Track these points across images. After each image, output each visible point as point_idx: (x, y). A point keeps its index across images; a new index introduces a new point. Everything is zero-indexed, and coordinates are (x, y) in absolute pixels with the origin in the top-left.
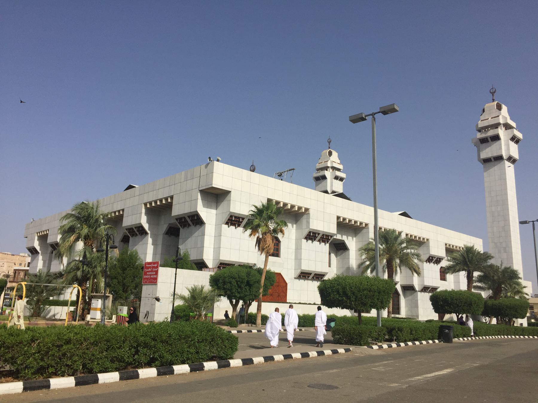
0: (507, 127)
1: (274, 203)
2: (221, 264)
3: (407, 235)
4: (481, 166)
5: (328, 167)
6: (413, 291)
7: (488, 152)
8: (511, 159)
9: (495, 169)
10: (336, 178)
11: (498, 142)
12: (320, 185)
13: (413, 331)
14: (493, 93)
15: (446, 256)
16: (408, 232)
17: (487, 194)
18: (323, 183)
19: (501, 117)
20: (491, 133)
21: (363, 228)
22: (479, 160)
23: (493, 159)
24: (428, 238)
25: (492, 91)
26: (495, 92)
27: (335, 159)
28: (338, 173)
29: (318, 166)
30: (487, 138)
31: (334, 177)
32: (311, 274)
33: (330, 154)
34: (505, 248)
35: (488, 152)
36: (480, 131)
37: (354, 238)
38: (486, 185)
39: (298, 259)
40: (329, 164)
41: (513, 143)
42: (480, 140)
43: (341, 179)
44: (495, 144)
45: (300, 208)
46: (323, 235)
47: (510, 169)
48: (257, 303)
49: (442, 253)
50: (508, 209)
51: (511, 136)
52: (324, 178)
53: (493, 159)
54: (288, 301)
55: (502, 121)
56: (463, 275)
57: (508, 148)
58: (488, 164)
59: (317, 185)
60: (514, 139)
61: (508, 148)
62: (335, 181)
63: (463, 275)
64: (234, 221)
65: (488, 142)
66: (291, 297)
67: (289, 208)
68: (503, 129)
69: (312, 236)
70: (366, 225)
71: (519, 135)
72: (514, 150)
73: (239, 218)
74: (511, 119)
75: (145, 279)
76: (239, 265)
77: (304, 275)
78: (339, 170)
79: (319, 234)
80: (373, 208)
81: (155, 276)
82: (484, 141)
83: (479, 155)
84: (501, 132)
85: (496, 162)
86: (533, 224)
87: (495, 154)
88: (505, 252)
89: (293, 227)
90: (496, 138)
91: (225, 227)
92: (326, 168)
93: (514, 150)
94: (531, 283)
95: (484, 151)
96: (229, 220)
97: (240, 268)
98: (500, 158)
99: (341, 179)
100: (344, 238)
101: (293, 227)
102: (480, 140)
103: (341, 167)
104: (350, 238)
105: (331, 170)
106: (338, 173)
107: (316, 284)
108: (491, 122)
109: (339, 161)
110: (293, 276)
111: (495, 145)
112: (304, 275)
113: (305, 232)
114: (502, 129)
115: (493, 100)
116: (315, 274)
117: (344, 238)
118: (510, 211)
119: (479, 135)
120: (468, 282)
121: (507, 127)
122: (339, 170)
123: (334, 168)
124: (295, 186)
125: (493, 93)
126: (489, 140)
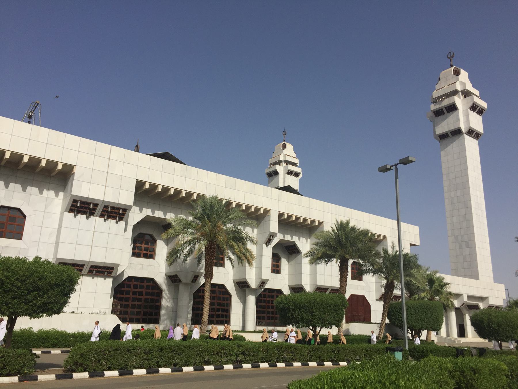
0: (466, 94)
4: (437, 143)
5: (281, 161)
7: (444, 126)
8: (471, 132)
9: (453, 146)
10: (290, 173)
11: (455, 113)
12: (273, 182)
13: (239, 351)
14: (451, 58)
15: (279, 231)
16: (283, 211)
17: (445, 177)
18: (275, 179)
19: (458, 83)
20: (446, 102)
21: (381, 241)
22: (435, 136)
23: (450, 134)
24: (321, 220)
25: (449, 56)
26: (452, 57)
27: (289, 152)
28: (291, 168)
29: (272, 161)
30: (442, 109)
31: (287, 171)
33: (284, 147)
34: (467, 242)
35: (444, 126)
36: (434, 102)
37: (309, 240)
38: (444, 166)
40: (282, 158)
41: (475, 114)
42: (434, 112)
43: (297, 175)
44: (452, 116)
45: (313, 222)
47: (471, 146)
49: (126, 197)
50: (469, 194)
51: (470, 104)
52: (276, 173)
53: (450, 134)
54: (372, 321)
55: (459, 88)
56: (334, 265)
57: (468, 119)
58: (447, 140)
59: (270, 182)
60: (474, 107)
61: (468, 119)
62: (288, 177)
63: (334, 265)
64: (111, 212)
65: (444, 114)
67: (309, 223)
68: (462, 97)
69: (82, 207)
70: (267, 212)
71: (483, 104)
72: (476, 122)
74: (473, 86)
76: (60, 263)
78: (294, 164)
80: (396, 222)
82: (439, 113)
83: (435, 132)
84: (459, 101)
85: (454, 138)
86: (397, 170)
87: (452, 128)
88: (468, 246)
89: (307, 241)
90: (453, 108)
92: (279, 163)
93: (476, 122)
94: (503, 285)
95: (440, 126)
97: (61, 267)
98: (458, 132)
99: (297, 175)
100: (295, 239)
101: (307, 241)
102: (434, 112)
103: (296, 161)
104: (303, 239)
105: (284, 165)
106: (291, 168)
107: (109, 282)
108: (447, 89)
109: (295, 155)
110: (375, 299)
111: (451, 117)
114: (459, 97)
115: (452, 66)
116: (92, 267)
117: (295, 239)
118: (472, 196)
119: (433, 107)
120: (341, 275)
121: (466, 94)
122: (294, 164)
123: (287, 162)
124: (223, 177)
125: (451, 58)
126: (445, 111)
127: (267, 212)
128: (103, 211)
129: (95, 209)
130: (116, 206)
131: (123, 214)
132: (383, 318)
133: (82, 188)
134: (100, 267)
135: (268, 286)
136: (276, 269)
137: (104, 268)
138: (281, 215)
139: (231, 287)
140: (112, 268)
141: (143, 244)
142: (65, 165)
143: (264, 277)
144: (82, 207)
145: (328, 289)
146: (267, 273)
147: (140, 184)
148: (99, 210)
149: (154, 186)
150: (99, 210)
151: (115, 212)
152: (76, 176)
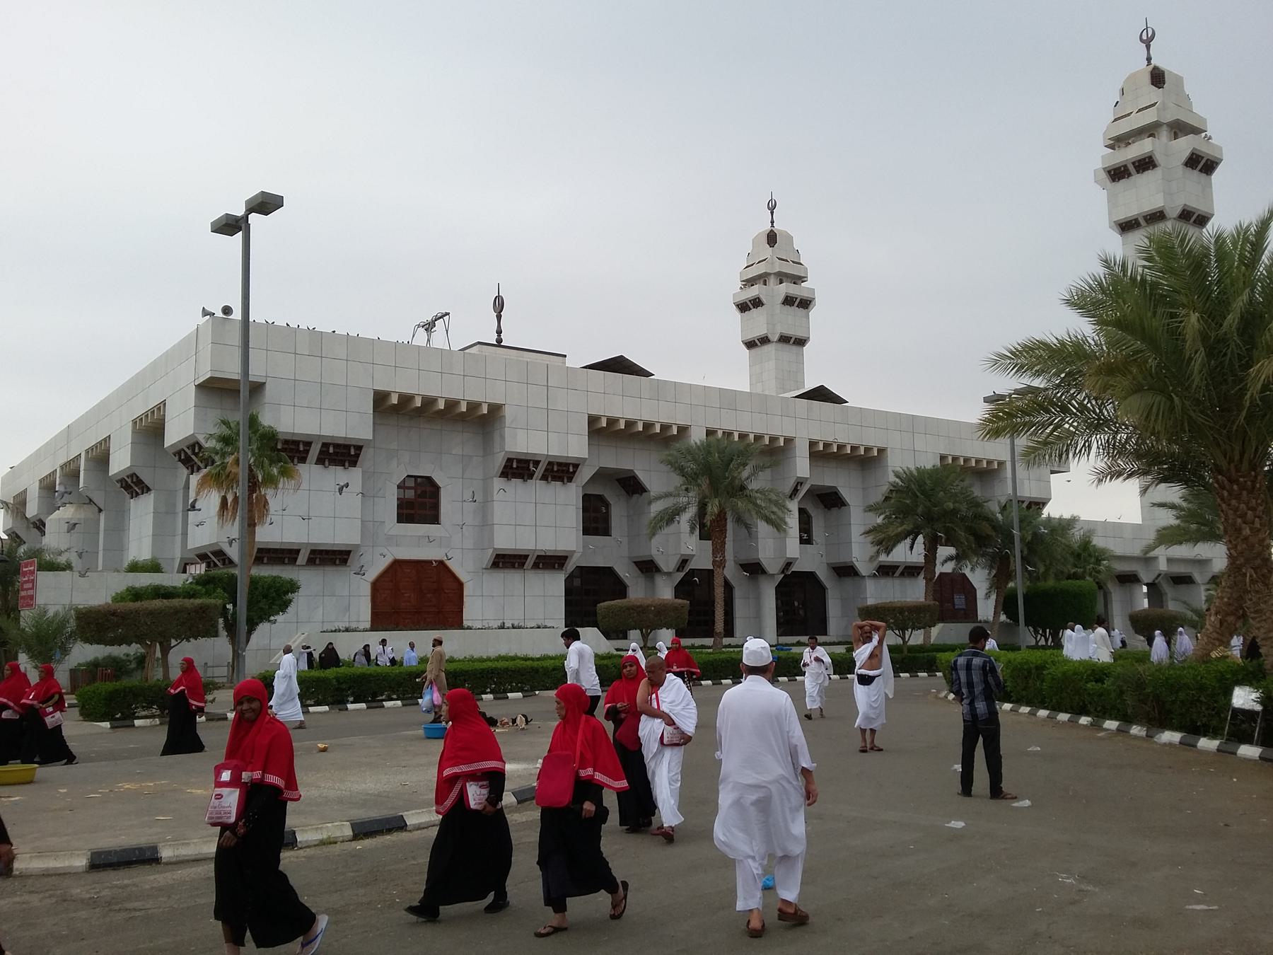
1: (736, 438)
2: (498, 556)
3: (710, 432)
6: (856, 578)
16: (815, 437)
21: (994, 470)
30: (1136, 220)
32: (526, 557)
39: (485, 525)
46: (550, 463)
48: (638, 631)
53: (1142, 222)
54: (466, 623)
65: (1130, 175)
66: (473, 610)
69: (519, 468)
73: (567, 465)
75: (23, 597)
77: (507, 561)
79: (537, 463)
81: (30, 592)
91: (498, 483)
96: (505, 467)
112: (507, 561)
113: (499, 462)
116: (313, 552)
127: (789, 441)
128: (321, 452)
129: (307, 452)
130: (289, 438)
131: (357, 456)
132: (996, 614)
133: (522, 440)
134: (327, 552)
135: (794, 568)
136: (806, 538)
137: (282, 551)
138: (813, 444)
139: (823, 574)
140: (565, 558)
141: (595, 519)
142: (490, 405)
143: (685, 551)
144: (519, 468)
145: (298, 551)
146: (793, 547)
147: (380, 399)
148: (315, 451)
149: (612, 421)
150: (315, 451)
151: (561, 471)
152: (508, 421)
